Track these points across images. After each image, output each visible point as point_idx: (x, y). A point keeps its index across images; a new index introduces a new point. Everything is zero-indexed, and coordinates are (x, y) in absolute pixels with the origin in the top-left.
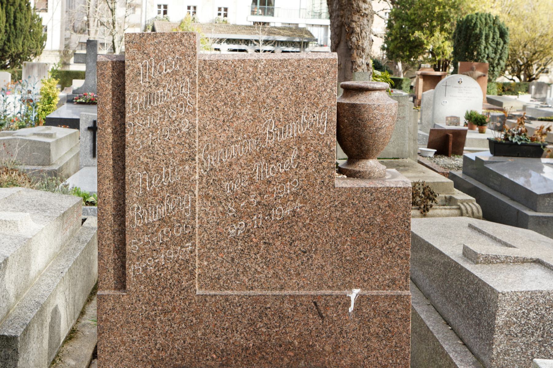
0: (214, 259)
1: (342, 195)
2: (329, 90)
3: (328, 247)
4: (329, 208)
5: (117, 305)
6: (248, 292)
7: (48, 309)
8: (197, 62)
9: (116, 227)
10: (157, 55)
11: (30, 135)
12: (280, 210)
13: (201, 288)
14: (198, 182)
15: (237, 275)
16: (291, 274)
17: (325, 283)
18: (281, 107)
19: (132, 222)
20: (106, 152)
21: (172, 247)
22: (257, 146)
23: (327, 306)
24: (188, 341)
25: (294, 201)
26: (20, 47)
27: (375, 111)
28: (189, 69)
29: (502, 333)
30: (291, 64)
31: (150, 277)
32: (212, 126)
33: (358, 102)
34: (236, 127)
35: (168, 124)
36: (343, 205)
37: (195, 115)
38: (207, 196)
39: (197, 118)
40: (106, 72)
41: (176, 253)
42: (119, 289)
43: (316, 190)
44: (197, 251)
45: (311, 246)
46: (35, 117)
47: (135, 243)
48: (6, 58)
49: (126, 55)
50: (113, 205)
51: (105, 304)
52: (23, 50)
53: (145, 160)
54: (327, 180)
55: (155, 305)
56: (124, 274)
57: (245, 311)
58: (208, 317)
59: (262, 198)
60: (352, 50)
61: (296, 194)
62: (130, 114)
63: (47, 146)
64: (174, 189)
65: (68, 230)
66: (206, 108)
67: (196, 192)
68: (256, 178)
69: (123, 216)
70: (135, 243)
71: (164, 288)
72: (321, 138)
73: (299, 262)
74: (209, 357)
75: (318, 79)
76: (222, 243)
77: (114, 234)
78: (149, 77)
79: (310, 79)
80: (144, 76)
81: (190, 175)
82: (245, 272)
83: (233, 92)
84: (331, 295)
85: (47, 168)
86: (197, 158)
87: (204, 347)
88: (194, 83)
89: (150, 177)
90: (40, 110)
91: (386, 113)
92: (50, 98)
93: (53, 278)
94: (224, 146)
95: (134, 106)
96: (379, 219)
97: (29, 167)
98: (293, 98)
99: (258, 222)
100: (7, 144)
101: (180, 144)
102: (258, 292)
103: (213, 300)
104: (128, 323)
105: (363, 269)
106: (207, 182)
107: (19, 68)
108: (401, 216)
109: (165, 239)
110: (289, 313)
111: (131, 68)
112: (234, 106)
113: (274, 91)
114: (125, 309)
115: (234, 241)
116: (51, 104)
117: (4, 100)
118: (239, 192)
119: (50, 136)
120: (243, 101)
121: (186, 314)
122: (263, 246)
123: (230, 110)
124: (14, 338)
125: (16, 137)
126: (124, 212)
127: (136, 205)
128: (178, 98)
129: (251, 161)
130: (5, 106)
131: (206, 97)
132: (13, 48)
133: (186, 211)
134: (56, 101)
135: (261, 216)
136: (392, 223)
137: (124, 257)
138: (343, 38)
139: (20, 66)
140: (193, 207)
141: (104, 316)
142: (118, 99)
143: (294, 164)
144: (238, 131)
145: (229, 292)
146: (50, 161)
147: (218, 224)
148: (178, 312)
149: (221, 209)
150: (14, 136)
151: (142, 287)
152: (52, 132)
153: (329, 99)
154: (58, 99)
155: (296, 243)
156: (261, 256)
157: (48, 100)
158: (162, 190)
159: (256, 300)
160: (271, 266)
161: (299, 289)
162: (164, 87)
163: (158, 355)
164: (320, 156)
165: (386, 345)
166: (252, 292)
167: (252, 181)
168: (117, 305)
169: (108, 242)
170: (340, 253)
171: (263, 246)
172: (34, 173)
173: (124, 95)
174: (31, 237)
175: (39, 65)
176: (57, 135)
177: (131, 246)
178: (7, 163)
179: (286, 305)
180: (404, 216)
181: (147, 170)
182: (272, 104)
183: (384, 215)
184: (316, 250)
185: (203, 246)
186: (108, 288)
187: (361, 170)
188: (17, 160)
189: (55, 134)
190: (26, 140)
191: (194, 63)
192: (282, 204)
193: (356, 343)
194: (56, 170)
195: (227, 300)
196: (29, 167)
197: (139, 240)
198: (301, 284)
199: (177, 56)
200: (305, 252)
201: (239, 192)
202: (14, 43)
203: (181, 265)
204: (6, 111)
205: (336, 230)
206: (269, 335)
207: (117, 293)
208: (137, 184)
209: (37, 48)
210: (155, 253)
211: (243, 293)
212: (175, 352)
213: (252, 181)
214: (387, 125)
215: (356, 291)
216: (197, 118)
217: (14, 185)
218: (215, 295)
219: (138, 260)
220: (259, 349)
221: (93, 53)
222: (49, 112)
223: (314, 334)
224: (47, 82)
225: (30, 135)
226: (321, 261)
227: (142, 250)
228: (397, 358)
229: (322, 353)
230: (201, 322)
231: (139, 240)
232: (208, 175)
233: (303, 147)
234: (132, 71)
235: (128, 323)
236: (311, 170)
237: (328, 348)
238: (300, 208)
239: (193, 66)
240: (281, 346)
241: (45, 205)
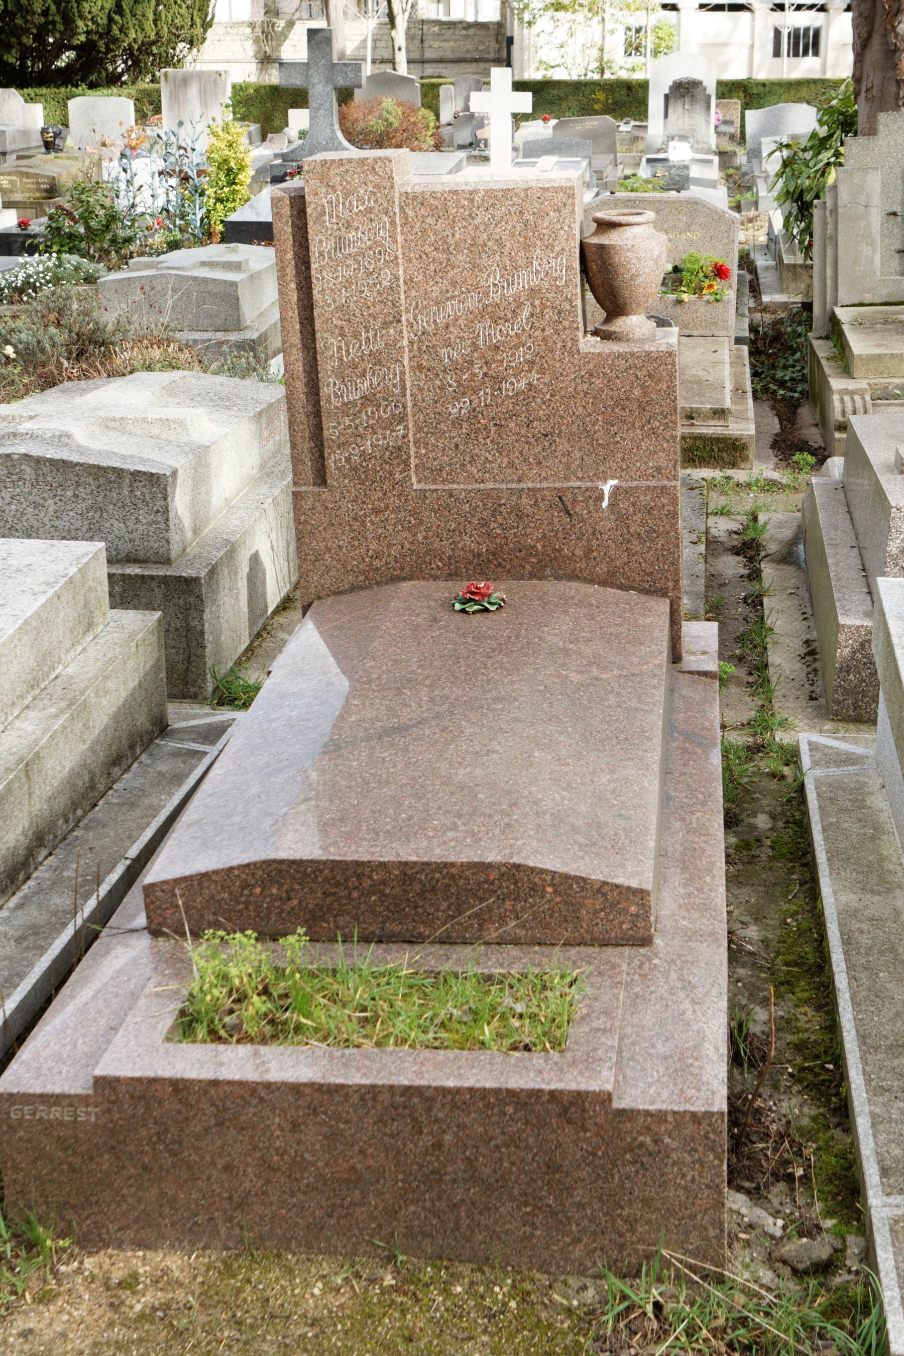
0: (433, 445)
1: (589, 362)
2: (566, 228)
3: (574, 428)
4: (574, 379)
5: (318, 504)
6: (477, 486)
7: (243, 552)
8: (397, 195)
9: (310, 408)
10: (344, 188)
11: (194, 266)
12: (512, 383)
13: (419, 482)
14: (407, 349)
15: (463, 465)
16: (530, 463)
17: (573, 473)
18: (506, 251)
19: (328, 400)
20: (290, 314)
21: (380, 431)
22: (479, 301)
23: (574, 501)
24: (407, 546)
25: (530, 371)
26: (149, 26)
27: (629, 254)
28: (386, 205)
29: (896, 565)
30: (516, 195)
31: (355, 469)
32: (421, 277)
33: (607, 242)
34: (452, 279)
35: (365, 277)
36: (591, 375)
37: (397, 265)
38: (420, 367)
39: (401, 268)
40: (283, 211)
41: (385, 438)
42: (319, 485)
43: (557, 357)
44: (410, 436)
45: (553, 428)
46: (202, 220)
47: (334, 427)
48: (116, 56)
49: (306, 190)
50: (304, 380)
51: (303, 502)
52: (157, 34)
53: (339, 323)
54: (569, 344)
55: (363, 503)
56: (323, 466)
57: (475, 509)
58: (429, 517)
59: (489, 369)
60: (897, 55)
61: (531, 363)
62: (317, 265)
63: (230, 290)
64: (377, 359)
65: (271, 442)
66: (412, 255)
67: (406, 363)
68: (481, 342)
69: (318, 394)
70: (334, 427)
71: (373, 482)
72: (559, 290)
73: (540, 448)
74: (433, 566)
75: (552, 213)
76: (443, 425)
77: (308, 416)
78: (337, 216)
79: (542, 214)
80: (331, 216)
81: (396, 341)
82: (472, 461)
83: (445, 234)
84: (579, 488)
85: (233, 337)
86: (403, 319)
87: (427, 553)
88: (393, 223)
89: (346, 344)
90: (212, 201)
91: (643, 255)
92: (229, 171)
93: (249, 511)
94: (437, 303)
95: (321, 254)
96: (637, 393)
97: (197, 336)
98: (521, 240)
99: (486, 399)
100: (147, 288)
101: (381, 302)
102: (490, 485)
103: (435, 495)
104: (332, 525)
105: (620, 455)
106: (419, 349)
107: (152, 81)
108: (664, 388)
109: (371, 422)
110: (528, 510)
111: (313, 206)
112: (447, 251)
113: (497, 230)
114: (327, 508)
115: (457, 422)
116: (235, 184)
117: (128, 181)
118: (460, 361)
119: (236, 267)
120: (457, 245)
121: (403, 514)
122: (493, 429)
123: (442, 257)
124: (196, 580)
125: (166, 272)
126: (318, 389)
127: (331, 380)
128: (375, 242)
129: (472, 321)
130: (131, 195)
131: (412, 241)
132: (133, 31)
133: (394, 385)
134: (246, 177)
135: (488, 391)
136: (654, 396)
137: (322, 445)
138: (877, 25)
139: (154, 76)
140: (403, 381)
141: (302, 518)
142: (301, 245)
143: (527, 324)
144: (454, 283)
145: (455, 486)
146: (239, 321)
147: (436, 402)
148: (392, 512)
149: (438, 383)
150: (161, 269)
151: (347, 481)
152: (240, 259)
153: (567, 240)
154: (251, 172)
155: (535, 424)
156: (492, 441)
157: (228, 175)
158: (363, 360)
159: (487, 495)
160: (504, 454)
161: (541, 481)
162: (357, 229)
163: (371, 564)
164: (559, 313)
165: (650, 548)
166: (482, 486)
167: (475, 347)
168: (318, 504)
169: (301, 427)
170: (590, 435)
171: (493, 429)
172: (207, 347)
173: (307, 240)
174: (207, 444)
175: (200, 75)
176: (251, 263)
177: (330, 431)
178: (153, 326)
179: (525, 501)
180: (668, 387)
181: (342, 335)
182: (496, 248)
183: (643, 387)
184: (560, 432)
185: (419, 429)
186: (305, 484)
187: (617, 330)
188: (172, 320)
189: (247, 261)
190: (188, 278)
191: (393, 197)
192: (515, 376)
193: (613, 546)
194: (253, 341)
195: (451, 496)
196: (197, 336)
197: (339, 423)
198: (544, 475)
199: (370, 189)
200: (546, 436)
201: (460, 361)
202: (134, 15)
203: (392, 453)
204: (133, 206)
205: (584, 407)
206: (506, 538)
207: (317, 489)
208: (331, 353)
209: (192, 26)
210: (359, 439)
211: (470, 487)
212: (391, 559)
213: (475, 347)
214: (647, 270)
215: (613, 482)
216: (401, 268)
217: (174, 368)
218: (437, 490)
219: (339, 448)
220: (494, 555)
221: (323, 62)
222: (232, 205)
223: (560, 535)
224: (221, 133)
225: (194, 266)
226: (567, 446)
227: (343, 435)
228: (665, 563)
229: (572, 558)
230: (421, 523)
231: (339, 423)
232: (420, 341)
233: (537, 303)
234: (315, 209)
235: (332, 525)
236: (549, 331)
237: (579, 552)
238: (538, 380)
239: (391, 201)
240: (520, 551)
241: (229, 399)
